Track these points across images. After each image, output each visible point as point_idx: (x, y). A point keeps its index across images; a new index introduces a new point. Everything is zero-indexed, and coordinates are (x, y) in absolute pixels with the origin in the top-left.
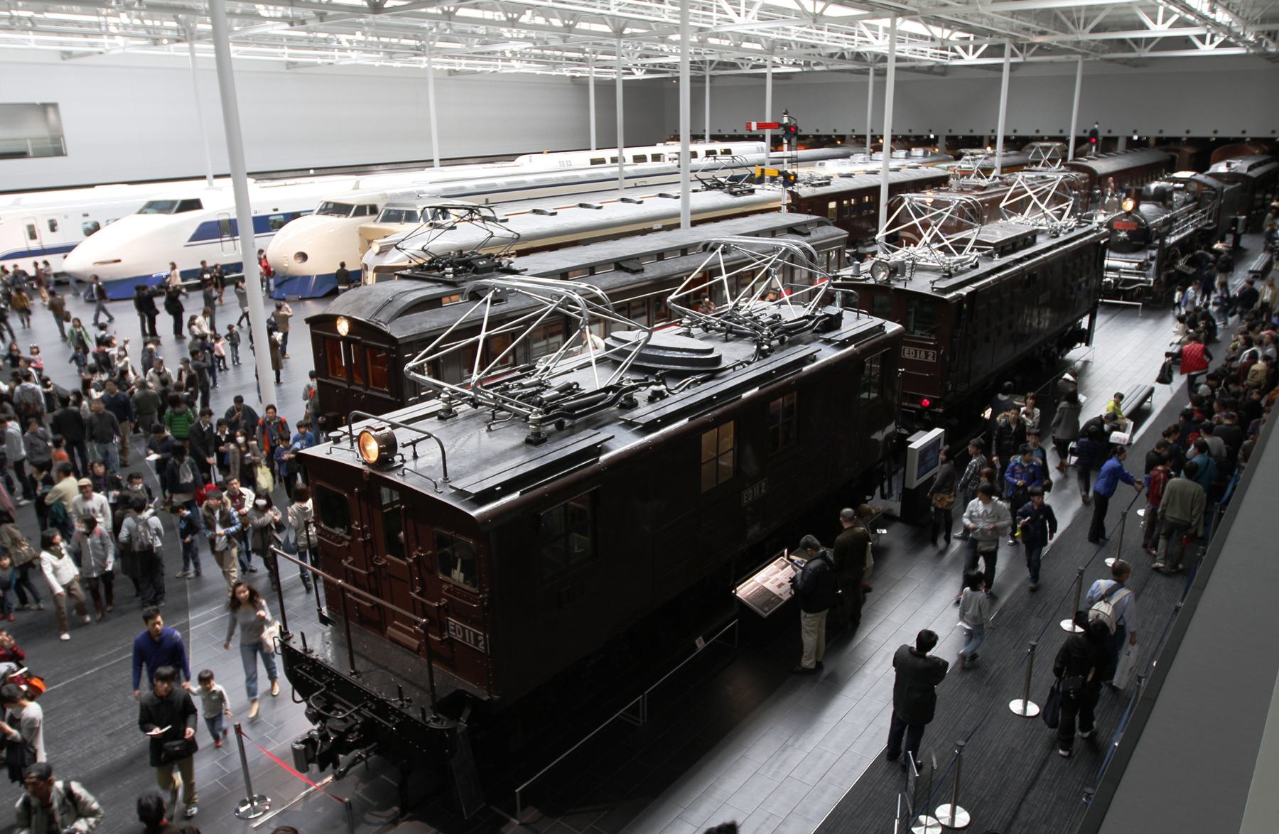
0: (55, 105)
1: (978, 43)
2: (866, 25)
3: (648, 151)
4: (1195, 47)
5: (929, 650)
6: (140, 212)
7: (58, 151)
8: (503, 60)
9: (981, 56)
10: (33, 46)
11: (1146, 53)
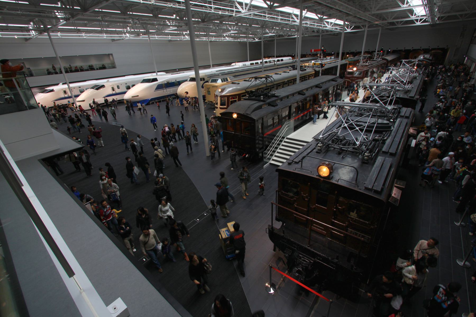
0: (112, 54)
2: (326, 22)
4: (410, 17)
6: (141, 83)
7: (114, 67)
10: (105, 38)
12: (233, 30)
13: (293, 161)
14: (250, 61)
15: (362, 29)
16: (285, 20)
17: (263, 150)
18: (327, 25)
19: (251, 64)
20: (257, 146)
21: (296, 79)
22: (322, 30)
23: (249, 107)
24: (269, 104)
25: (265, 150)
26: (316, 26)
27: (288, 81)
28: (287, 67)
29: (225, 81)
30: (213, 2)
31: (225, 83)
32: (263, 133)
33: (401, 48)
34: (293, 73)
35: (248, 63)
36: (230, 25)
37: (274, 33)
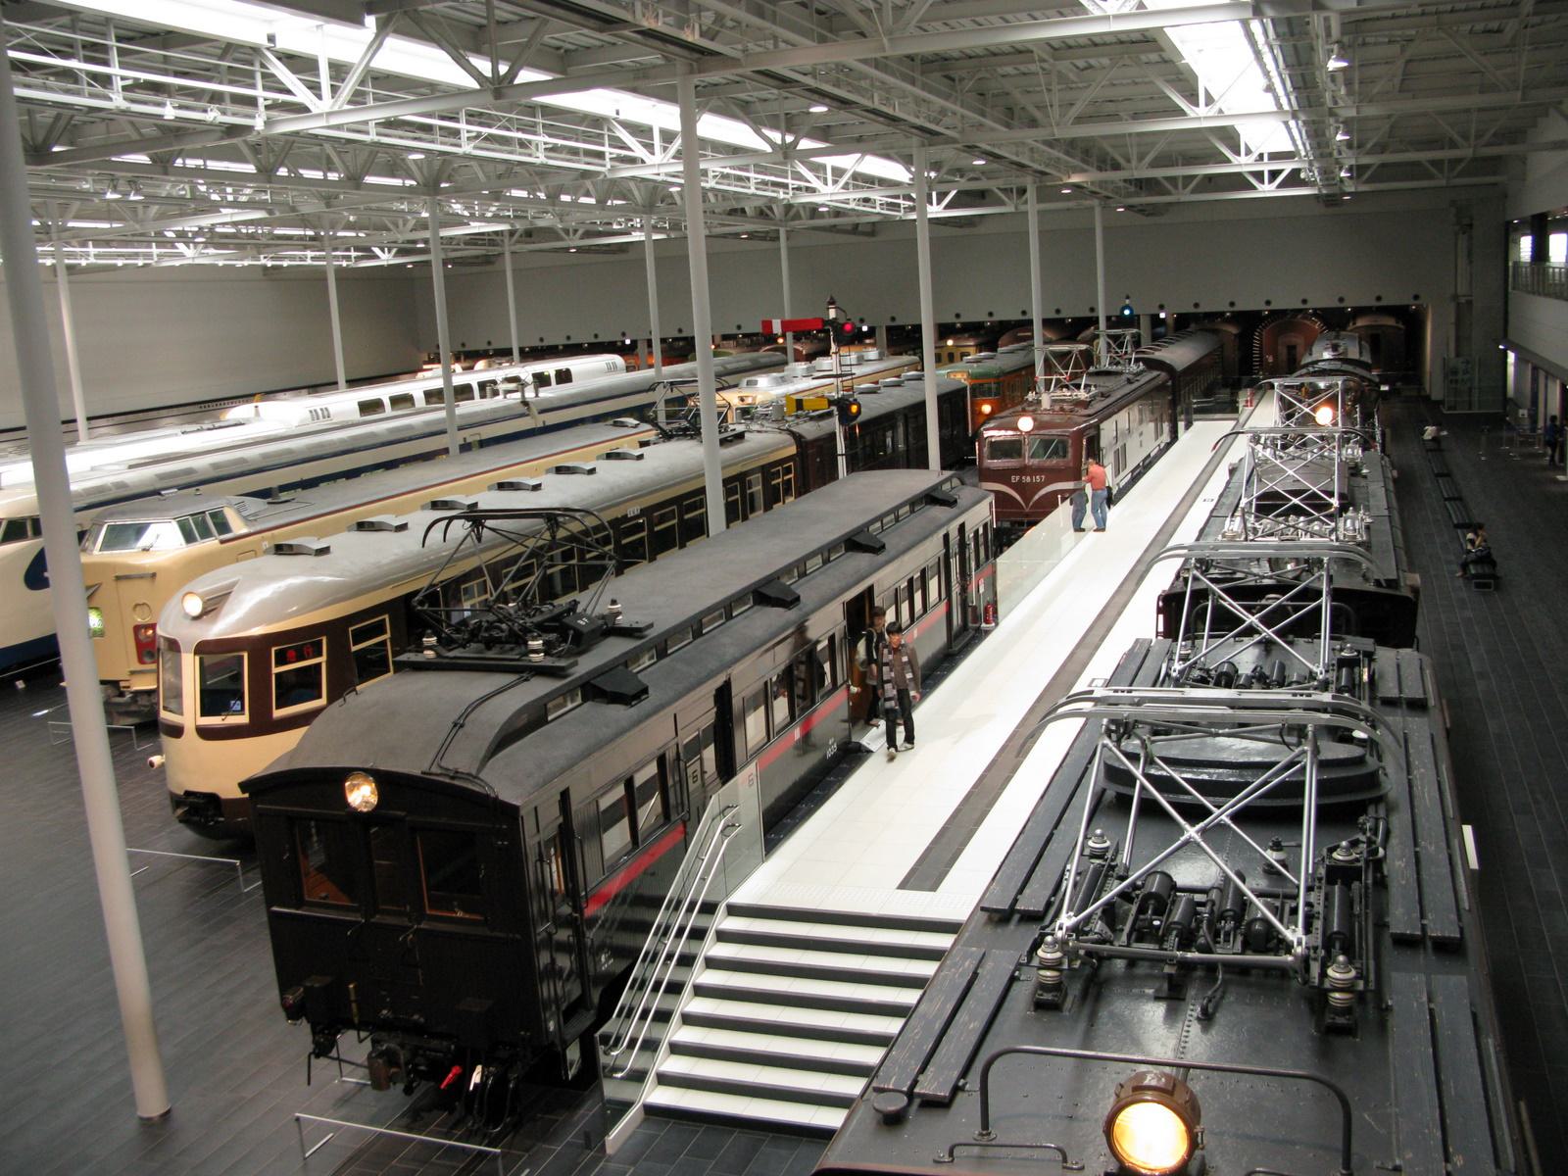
1: (943, 188)
3: (383, 392)
4: (1254, 188)
5: (1408, 598)
8: (160, 245)
9: (947, 207)
11: (1186, 196)
12: (235, 204)
13: (910, 1094)
14: (354, 383)
15: (1002, 203)
16: (574, 152)
17: (586, 1020)
18: (815, 183)
19: (367, 407)
20: (546, 990)
21: (702, 491)
22: (789, 207)
23: (458, 725)
24: (593, 690)
25: (604, 1015)
26: (753, 186)
27: (644, 512)
28: (612, 417)
29: (206, 534)
30: (122, 52)
31: (211, 544)
32: (572, 893)
33: (1215, 302)
34: (667, 460)
35: (344, 403)
36: (219, 179)
37: (496, 218)
